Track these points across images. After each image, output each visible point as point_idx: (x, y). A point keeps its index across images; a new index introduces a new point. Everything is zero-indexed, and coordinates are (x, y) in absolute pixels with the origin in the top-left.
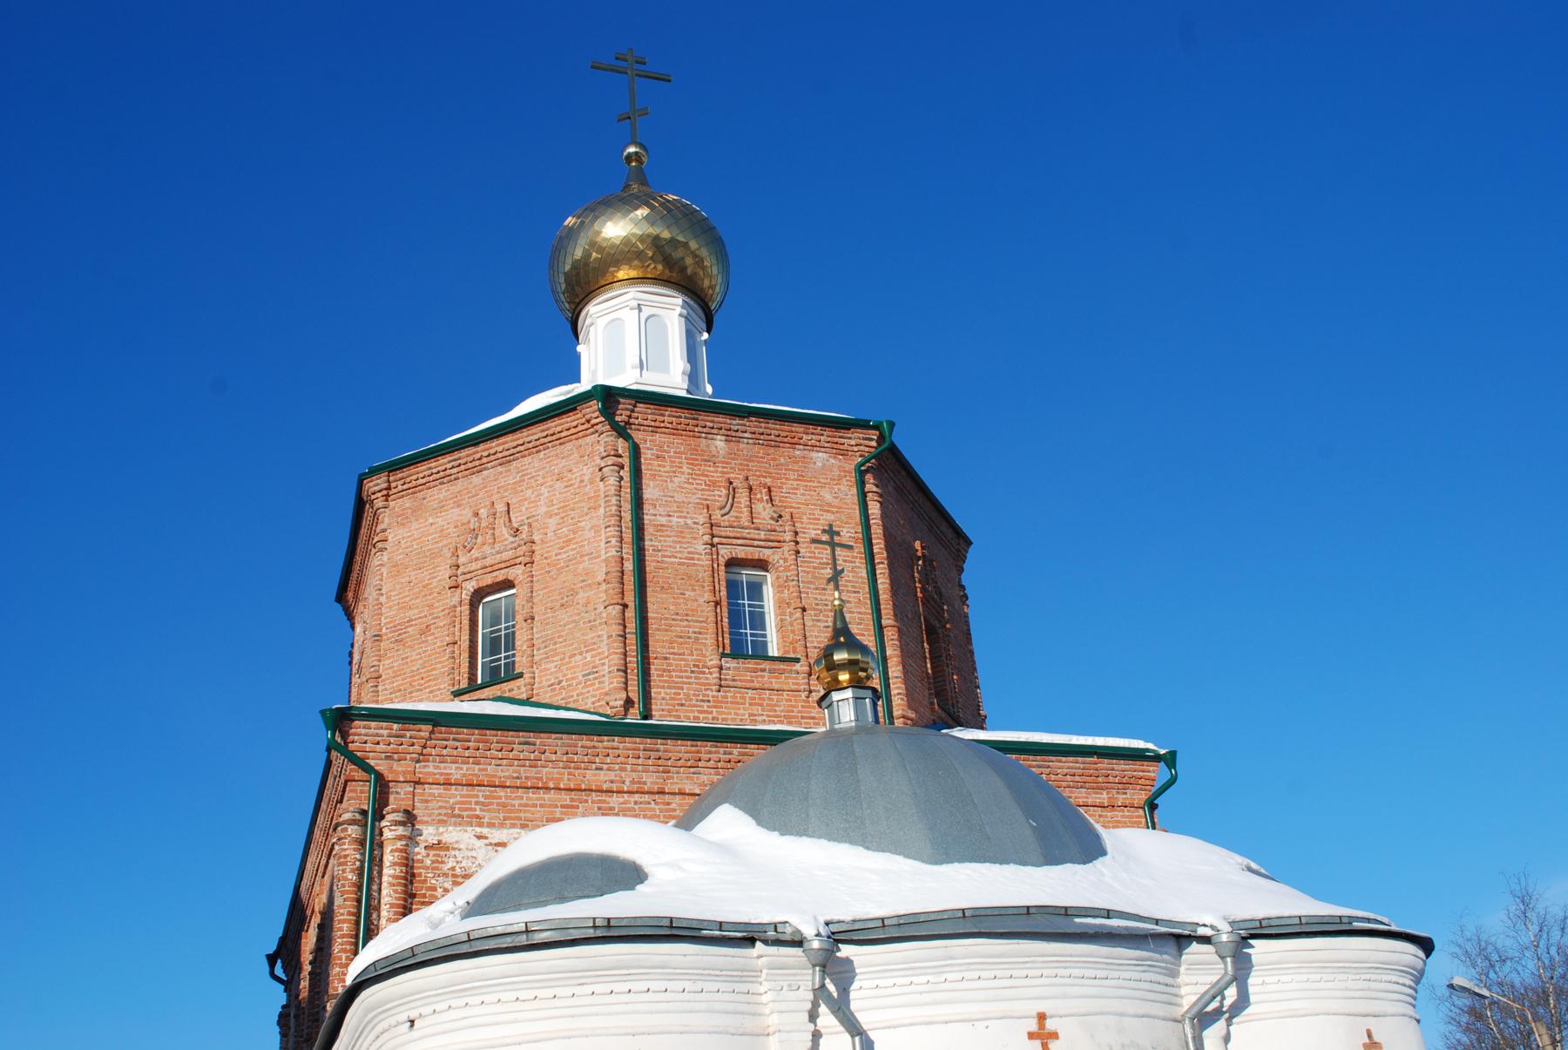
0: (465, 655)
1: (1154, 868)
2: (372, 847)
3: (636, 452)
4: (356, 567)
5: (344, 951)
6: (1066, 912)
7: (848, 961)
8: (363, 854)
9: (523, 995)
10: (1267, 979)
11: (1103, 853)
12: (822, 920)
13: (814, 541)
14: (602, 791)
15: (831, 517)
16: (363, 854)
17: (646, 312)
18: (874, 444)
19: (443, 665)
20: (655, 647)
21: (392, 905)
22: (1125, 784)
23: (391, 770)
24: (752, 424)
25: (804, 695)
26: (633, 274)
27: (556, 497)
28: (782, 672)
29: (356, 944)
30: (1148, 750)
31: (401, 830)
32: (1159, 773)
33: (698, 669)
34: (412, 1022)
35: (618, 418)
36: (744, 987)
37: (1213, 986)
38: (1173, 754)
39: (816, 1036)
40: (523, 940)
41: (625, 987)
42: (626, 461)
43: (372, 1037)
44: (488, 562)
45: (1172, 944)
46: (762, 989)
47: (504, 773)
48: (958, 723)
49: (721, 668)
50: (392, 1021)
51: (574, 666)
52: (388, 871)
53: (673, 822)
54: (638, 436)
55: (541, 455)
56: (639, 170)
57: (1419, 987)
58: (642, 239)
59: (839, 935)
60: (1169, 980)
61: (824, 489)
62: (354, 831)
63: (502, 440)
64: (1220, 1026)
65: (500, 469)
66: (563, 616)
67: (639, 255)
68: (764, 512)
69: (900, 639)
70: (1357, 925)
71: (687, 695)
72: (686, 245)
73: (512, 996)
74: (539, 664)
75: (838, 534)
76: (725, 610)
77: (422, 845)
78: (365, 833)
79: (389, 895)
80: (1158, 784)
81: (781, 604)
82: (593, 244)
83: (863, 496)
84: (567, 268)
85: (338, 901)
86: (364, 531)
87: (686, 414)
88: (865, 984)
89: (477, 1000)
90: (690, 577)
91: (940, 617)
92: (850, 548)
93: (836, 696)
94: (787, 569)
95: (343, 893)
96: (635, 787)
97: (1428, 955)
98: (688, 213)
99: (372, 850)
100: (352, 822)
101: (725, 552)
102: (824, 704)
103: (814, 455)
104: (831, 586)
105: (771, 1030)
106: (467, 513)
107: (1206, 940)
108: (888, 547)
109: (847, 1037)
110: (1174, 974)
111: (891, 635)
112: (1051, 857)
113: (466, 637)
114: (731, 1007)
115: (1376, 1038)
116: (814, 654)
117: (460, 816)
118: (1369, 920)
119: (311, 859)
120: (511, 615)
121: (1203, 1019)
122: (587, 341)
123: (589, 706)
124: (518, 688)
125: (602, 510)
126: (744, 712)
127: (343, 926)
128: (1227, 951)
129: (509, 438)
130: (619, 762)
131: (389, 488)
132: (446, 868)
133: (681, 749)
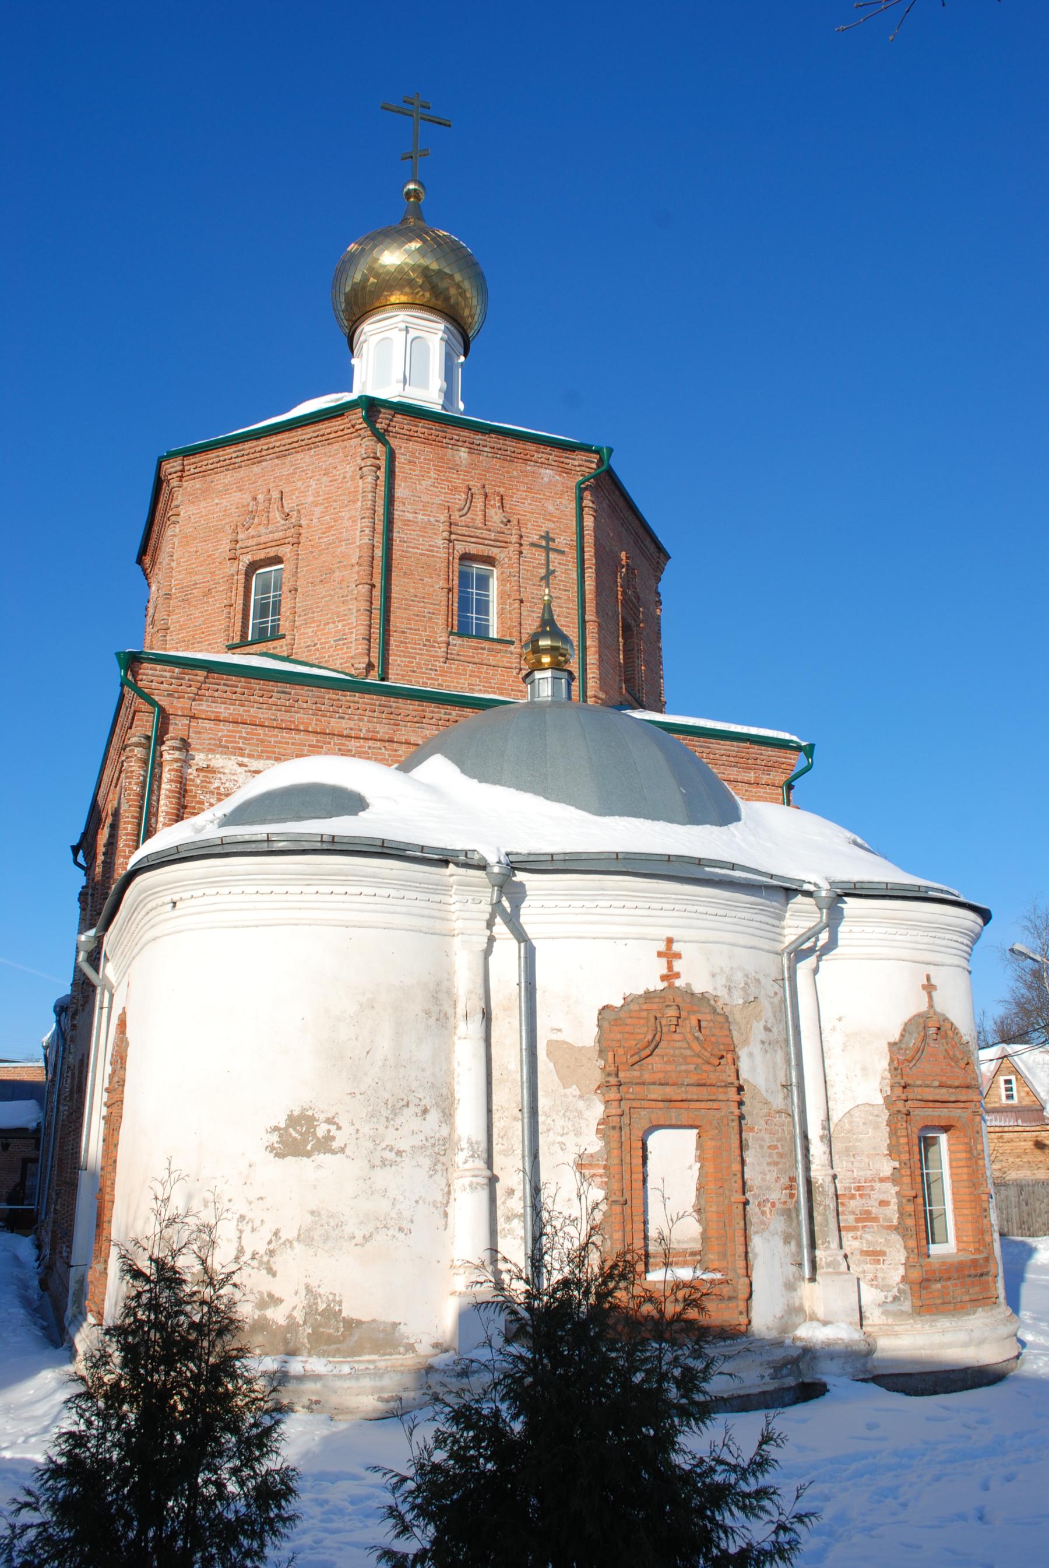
0: (239, 616)
1: (777, 836)
2: (154, 766)
3: (392, 456)
4: (154, 536)
5: (128, 846)
6: (700, 862)
7: (521, 885)
8: (146, 771)
9: (262, 889)
10: (854, 929)
11: (738, 819)
12: (503, 851)
13: (533, 545)
14: (342, 736)
15: (552, 525)
16: (146, 771)
17: (413, 333)
18: (594, 466)
19: (221, 624)
20: (395, 622)
21: (167, 813)
22: (769, 767)
23: (172, 706)
24: (492, 440)
25: (515, 672)
26: (404, 299)
27: (323, 490)
28: (500, 651)
29: (138, 842)
30: (792, 741)
31: (177, 754)
32: (799, 760)
33: (430, 643)
34: (175, 903)
35: (378, 426)
36: (438, 898)
37: (810, 929)
38: (812, 747)
39: (491, 940)
40: (264, 847)
41: (343, 889)
42: (383, 463)
43: (143, 913)
44: (262, 539)
45: (782, 895)
46: (451, 901)
47: (263, 715)
48: (641, 706)
49: (448, 644)
50: (159, 901)
51: (327, 633)
52: (165, 786)
53: (396, 765)
54: (394, 442)
55: (312, 452)
56: (417, 205)
57: (975, 947)
58: (413, 268)
59: (516, 864)
60: (776, 922)
61: (548, 500)
62: (139, 752)
63: (280, 436)
64: (811, 961)
65: (276, 461)
66: (322, 590)
67: (410, 283)
68: (496, 516)
69: (599, 632)
70: (932, 894)
71: (419, 664)
72: (451, 277)
73: (254, 889)
74: (299, 628)
75: (553, 540)
76: (456, 596)
77: (194, 768)
78: (148, 754)
79: (165, 805)
80: (796, 770)
81: (503, 595)
82: (371, 269)
83: (580, 509)
84: (348, 289)
85: (124, 807)
86: (161, 505)
87: (437, 426)
88: (533, 904)
89: (226, 890)
90: (429, 566)
91: (636, 618)
92: (562, 553)
93: (538, 675)
94: (510, 566)
95: (129, 801)
96: (370, 735)
97: (985, 923)
98: (456, 248)
99: (153, 768)
100: (138, 745)
101: (460, 548)
102: (528, 680)
103: (543, 471)
104: (543, 583)
105: (456, 932)
106: (247, 497)
107: (809, 894)
108: (597, 555)
109: (515, 942)
110: (781, 918)
111: (592, 628)
112: (694, 819)
113: (240, 601)
114: (426, 912)
115: (933, 982)
116: (525, 637)
117: (225, 747)
118: (942, 891)
119: (108, 772)
120: (278, 586)
121: (799, 954)
122: (360, 356)
123: (338, 666)
124: (280, 647)
125: (359, 504)
126: (464, 682)
127: (127, 828)
128: (825, 903)
129: (286, 435)
130: (358, 714)
131: (183, 471)
132: (212, 787)
133: (410, 707)
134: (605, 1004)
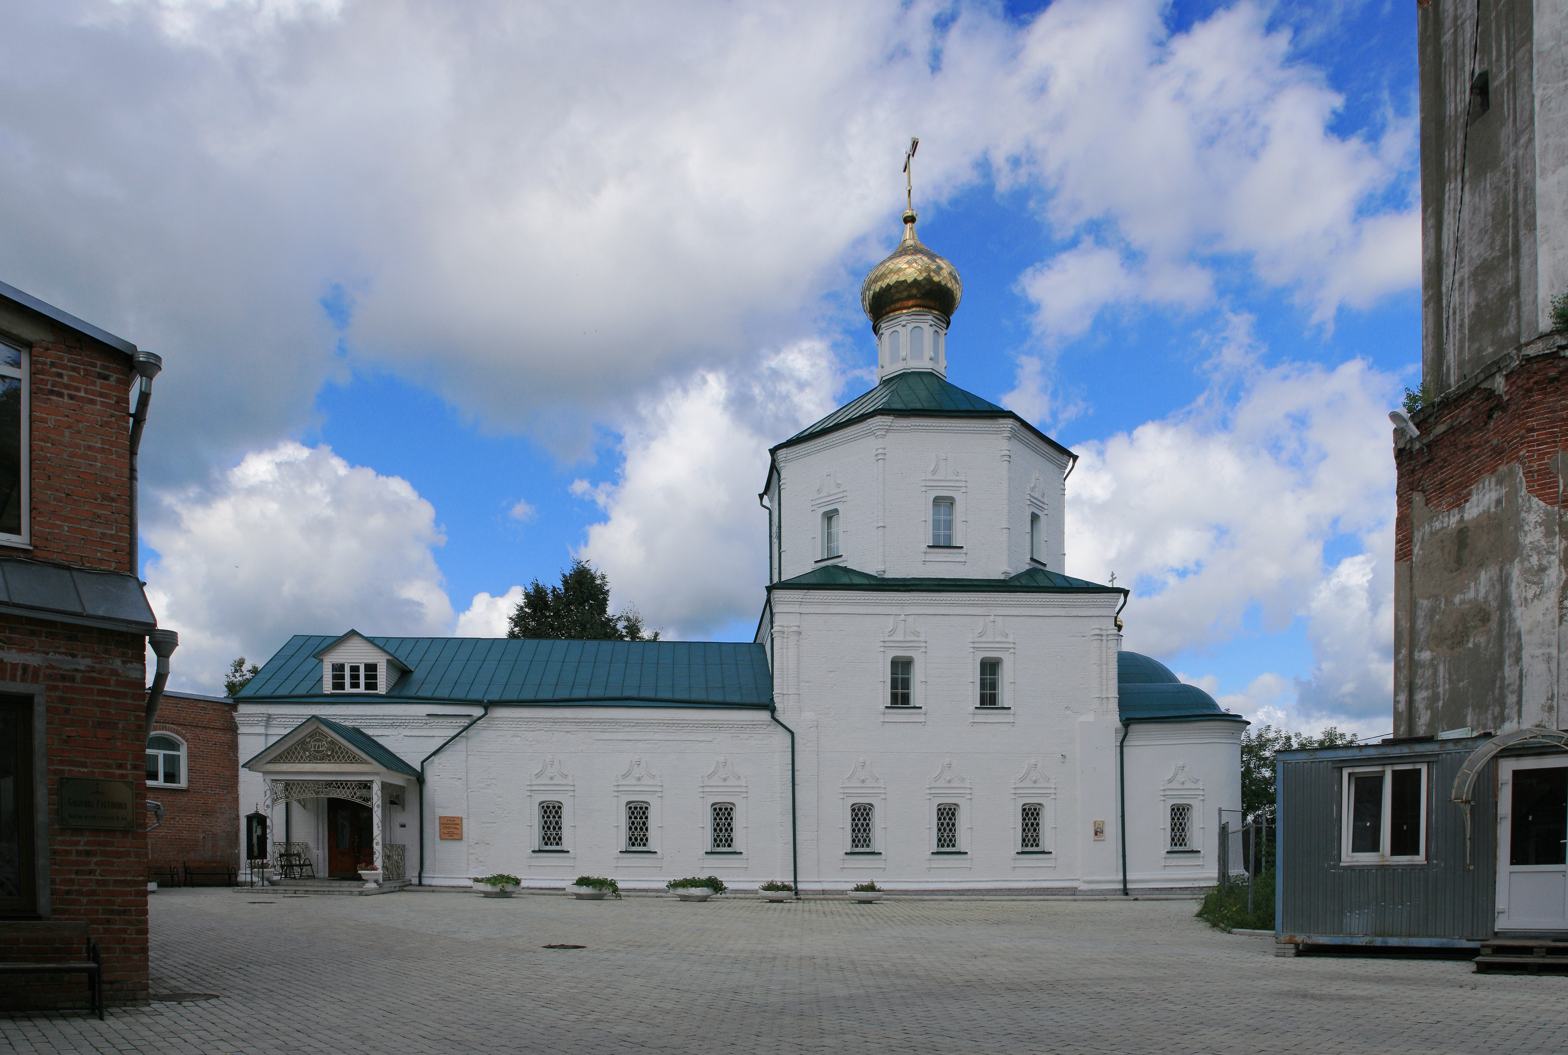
134: (585, 875)
